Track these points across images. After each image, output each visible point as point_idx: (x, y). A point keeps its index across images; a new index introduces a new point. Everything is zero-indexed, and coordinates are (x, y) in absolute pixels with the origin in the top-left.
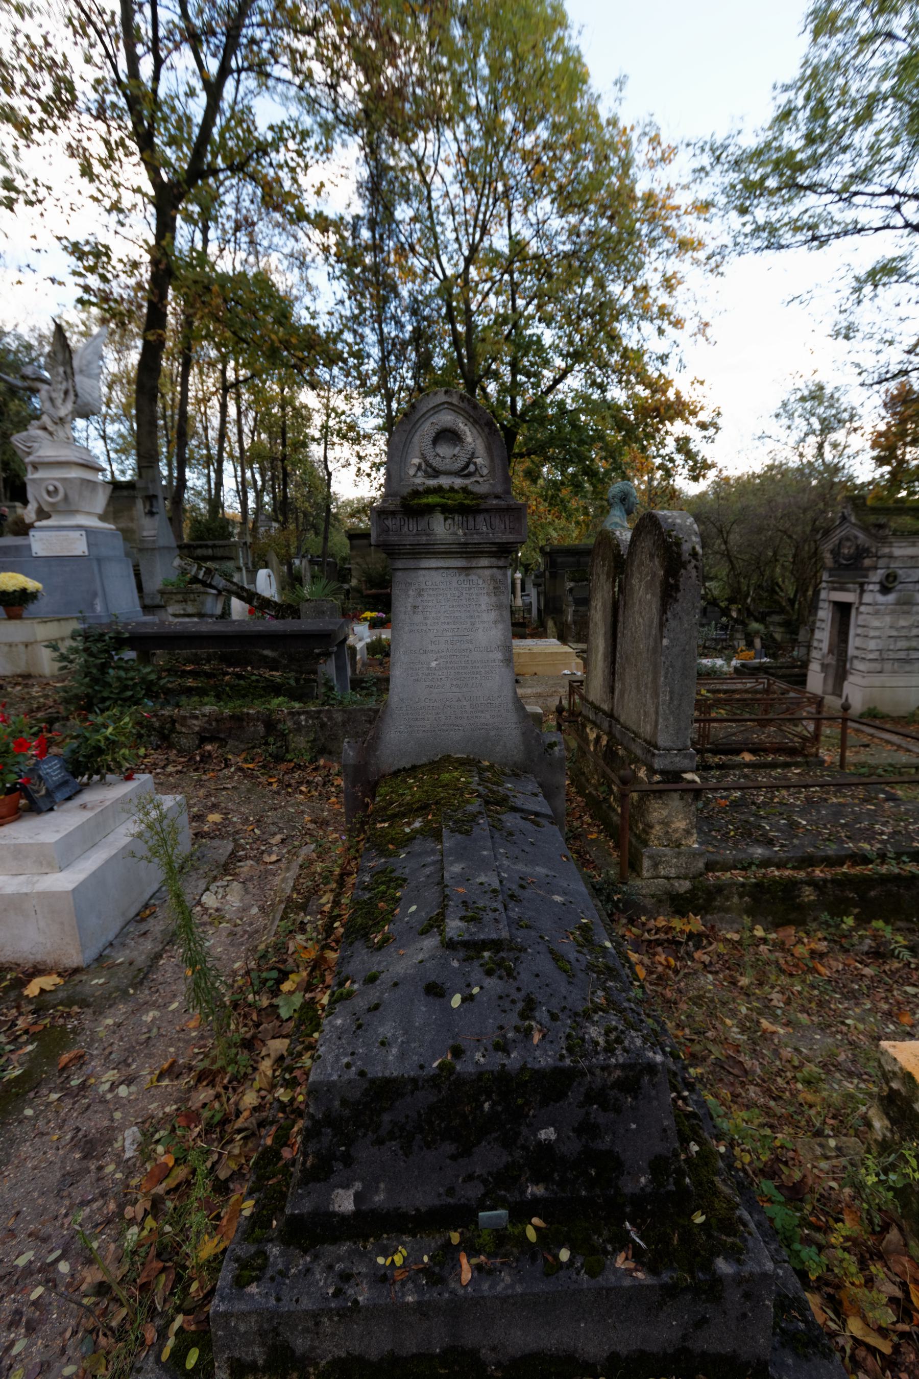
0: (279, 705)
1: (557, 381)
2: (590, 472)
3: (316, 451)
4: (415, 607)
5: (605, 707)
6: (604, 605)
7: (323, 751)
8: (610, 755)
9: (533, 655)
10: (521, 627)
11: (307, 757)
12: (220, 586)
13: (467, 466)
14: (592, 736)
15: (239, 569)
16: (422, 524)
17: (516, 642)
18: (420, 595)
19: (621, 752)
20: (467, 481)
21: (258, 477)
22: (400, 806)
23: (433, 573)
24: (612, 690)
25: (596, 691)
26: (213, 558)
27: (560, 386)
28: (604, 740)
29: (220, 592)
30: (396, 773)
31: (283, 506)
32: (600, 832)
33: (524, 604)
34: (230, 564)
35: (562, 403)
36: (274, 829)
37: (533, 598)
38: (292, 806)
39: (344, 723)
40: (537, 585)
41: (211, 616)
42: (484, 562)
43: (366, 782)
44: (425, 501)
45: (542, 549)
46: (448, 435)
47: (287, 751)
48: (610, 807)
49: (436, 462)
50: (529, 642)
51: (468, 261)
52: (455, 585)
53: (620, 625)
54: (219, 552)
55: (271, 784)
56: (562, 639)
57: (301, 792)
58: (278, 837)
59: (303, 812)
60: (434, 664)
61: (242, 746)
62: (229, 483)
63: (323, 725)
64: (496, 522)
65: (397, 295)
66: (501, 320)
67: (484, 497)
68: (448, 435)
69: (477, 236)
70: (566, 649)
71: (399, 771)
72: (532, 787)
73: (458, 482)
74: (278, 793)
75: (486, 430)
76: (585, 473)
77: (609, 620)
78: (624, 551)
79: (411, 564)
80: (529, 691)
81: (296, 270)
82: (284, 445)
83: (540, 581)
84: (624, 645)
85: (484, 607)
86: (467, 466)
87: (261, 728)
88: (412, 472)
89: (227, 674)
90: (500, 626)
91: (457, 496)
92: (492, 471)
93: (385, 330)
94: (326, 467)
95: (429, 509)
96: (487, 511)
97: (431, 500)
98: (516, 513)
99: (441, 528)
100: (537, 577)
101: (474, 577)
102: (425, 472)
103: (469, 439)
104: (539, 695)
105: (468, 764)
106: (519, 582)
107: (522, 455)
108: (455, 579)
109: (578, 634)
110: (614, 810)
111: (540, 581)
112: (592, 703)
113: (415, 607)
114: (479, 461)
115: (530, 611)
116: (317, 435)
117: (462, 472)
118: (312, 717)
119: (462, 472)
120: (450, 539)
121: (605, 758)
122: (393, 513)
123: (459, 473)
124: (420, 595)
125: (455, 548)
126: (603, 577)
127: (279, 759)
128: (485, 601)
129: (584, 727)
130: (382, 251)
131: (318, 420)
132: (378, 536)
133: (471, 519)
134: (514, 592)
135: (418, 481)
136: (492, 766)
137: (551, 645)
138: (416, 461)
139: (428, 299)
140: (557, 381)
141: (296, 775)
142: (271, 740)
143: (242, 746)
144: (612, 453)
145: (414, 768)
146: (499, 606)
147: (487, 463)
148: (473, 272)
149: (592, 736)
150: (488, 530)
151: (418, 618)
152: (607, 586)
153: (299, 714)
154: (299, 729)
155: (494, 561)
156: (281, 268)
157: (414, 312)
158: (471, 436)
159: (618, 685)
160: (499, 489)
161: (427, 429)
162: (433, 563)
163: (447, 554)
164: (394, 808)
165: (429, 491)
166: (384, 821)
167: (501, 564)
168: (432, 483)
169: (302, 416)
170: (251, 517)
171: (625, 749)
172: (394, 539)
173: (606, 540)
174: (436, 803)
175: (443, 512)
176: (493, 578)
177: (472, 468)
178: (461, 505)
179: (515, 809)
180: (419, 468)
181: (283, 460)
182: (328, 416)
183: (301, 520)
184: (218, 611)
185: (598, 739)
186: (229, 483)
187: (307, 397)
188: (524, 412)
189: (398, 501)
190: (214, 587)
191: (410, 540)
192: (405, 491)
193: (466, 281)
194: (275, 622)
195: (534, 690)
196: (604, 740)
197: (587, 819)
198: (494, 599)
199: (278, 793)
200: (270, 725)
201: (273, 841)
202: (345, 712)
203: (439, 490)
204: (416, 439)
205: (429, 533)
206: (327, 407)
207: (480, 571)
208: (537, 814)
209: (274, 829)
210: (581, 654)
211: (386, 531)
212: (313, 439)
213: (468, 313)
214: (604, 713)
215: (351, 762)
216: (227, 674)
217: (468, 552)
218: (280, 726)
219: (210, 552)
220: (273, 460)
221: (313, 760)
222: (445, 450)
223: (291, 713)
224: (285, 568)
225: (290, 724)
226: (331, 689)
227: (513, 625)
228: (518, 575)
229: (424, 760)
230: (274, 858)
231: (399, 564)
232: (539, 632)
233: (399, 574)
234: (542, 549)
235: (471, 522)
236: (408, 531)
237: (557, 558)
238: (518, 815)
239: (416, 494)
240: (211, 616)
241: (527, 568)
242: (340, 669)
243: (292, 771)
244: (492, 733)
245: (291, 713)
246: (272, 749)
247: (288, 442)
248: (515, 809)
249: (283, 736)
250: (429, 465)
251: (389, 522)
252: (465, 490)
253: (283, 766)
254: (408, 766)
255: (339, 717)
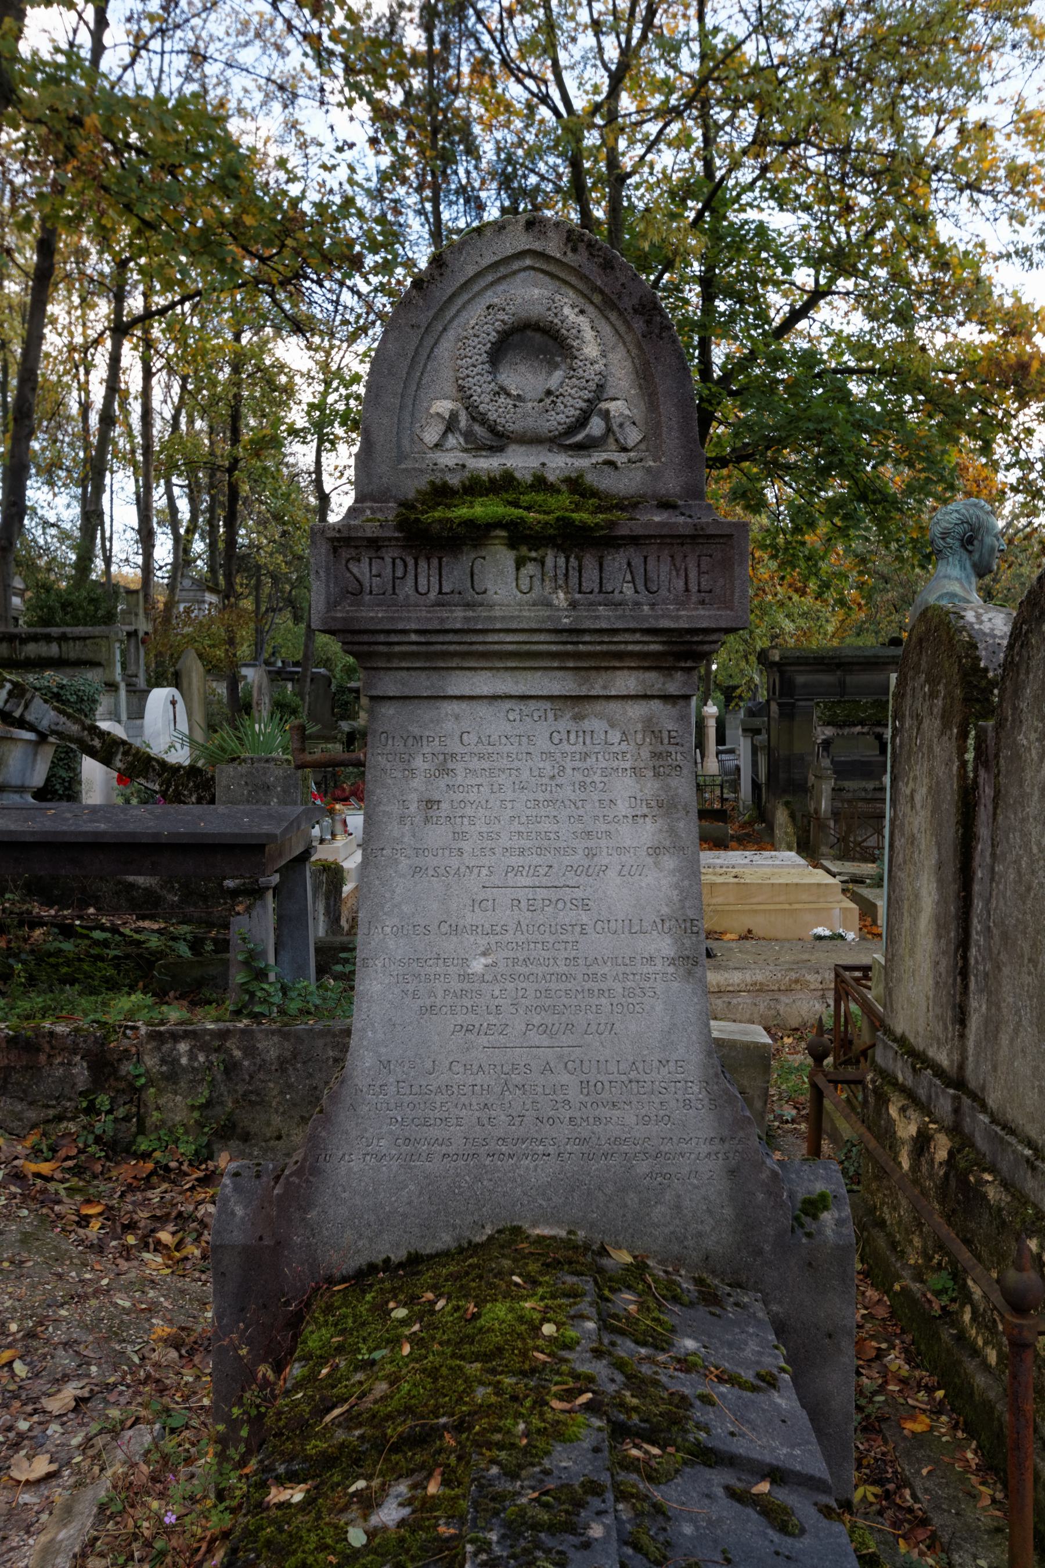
0: (131, 1015)
1: (796, 315)
2: (869, 493)
3: (301, 455)
4: (430, 803)
5: (943, 1058)
6: (935, 791)
7: (229, 1132)
8: (959, 1191)
9: (744, 888)
10: (722, 823)
11: (187, 1148)
12: (44, 725)
13: (583, 421)
14: (907, 1129)
15: (111, 686)
16: (455, 575)
17: (709, 857)
18: (444, 770)
19: (992, 1193)
20: (582, 462)
21: (183, 506)
22: (350, 1420)
23: (483, 710)
24: (961, 1018)
25: (915, 1005)
26: (58, 663)
27: (802, 325)
28: (941, 1149)
29: (43, 738)
30: (362, 1277)
31: (228, 559)
32: (937, 1410)
33: (724, 771)
34: (93, 676)
35: (809, 358)
36: (66, 1361)
37: (743, 759)
38: (128, 1288)
39: (283, 1065)
40: (751, 731)
41: (21, 789)
42: (627, 682)
43: (275, 1301)
44: (463, 512)
45: (762, 657)
46: (532, 339)
47: (141, 1130)
48: (961, 1337)
49: (497, 411)
50: (735, 858)
51: (617, 80)
52: (542, 743)
53: (982, 849)
54: (73, 651)
55: (84, 1221)
56: (807, 848)
57: (159, 1247)
58: (70, 1391)
59: (152, 1309)
60: (478, 965)
61: (32, 1115)
62: (121, 510)
63: (231, 1068)
64: (662, 571)
65: (473, 151)
66: (682, 193)
67: (630, 504)
68: (532, 339)
69: (637, 33)
70: (820, 876)
71: (372, 1268)
72: (758, 1350)
73: (558, 464)
74: (99, 1249)
75: (638, 324)
76: (863, 498)
77: (951, 833)
78: (991, 661)
79: (421, 683)
80: (736, 978)
81: (276, 106)
82: (235, 439)
83: (758, 722)
84: (997, 902)
85: (623, 808)
86: (583, 421)
87: (81, 1072)
88: (431, 436)
89: (36, 923)
90: (669, 862)
91: (552, 501)
92: (653, 433)
93: (445, 216)
94: (318, 483)
95: (475, 535)
96: (635, 540)
97: (481, 509)
98: (715, 547)
99: (507, 587)
100: (751, 713)
101: (596, 724)
102: (468, 435)
103: (591, 350)
104: (759, 989)
105: (571, 1261)
106: (712, 723)
107: (722, 462)
108: (542, 729)
109: (843, 839)
110: (976, 1352)
111: (758, 722)
112: (902, 1041)
113: (430, 803)
114: (615, 407)
115: (735, 786)
116: (301, 423)
117: (569, 438)
118: (204, 1048)
119: (569, 438)
120: (531, 617)
121: (943, 1195)
122: (375, 544)
123: (557, 441)
124: (444, 770)
125: (544, 643)
126: (932, 725)
127: (117, 1149)
128: (627, 790)
129: (883, 1100)
130: (447, 66)
131: (307, 393)
132: (332, 605)
133: (590, 562)
134: (700, 745)
135: (447, 460)
136: (640, 1267)
137: (783, 866)
138: (444, 406)
139: (535, 153)
140: (796, 315)
141: (154, 1196)
142: (103, 1100)
143: (32, 1115)
144: (918, 453)
145: (415, 1261)
146: (666, 806)
147: (638, 413)
148: (626, 103)
149: (907, 1129)
150: (636, 594)
151: (437, 835)
152: (943, 748)
153: (175, 1037)
154: (172, 1075)
155: (654, 681)
156: (247, 104)
157: (506, 181)
158: (592, 339)
159: (978, 1006)
160: (671, 484)
161: (477, 322)
162: (484, 683)
163: (524, 658)
164: (334, 1429)
165: (476, 487)
166: (292, 1478)
167: (673, 688)
168: (487, 464)
169: (276, 389)
170: (161, 577)
171: (1006, 1185)
172: (372, 614)
173: (940, 629)
174: (460, 1427)
175: (512, 544)
176: (651, 729)
177: (596, 426)
178: (564, 523)
179: (707, 1456)
180: (451, 425)
181: (231, 470)
182: (327, 383)
183: (266, 590)
184: (38, 778)
185: (922, 1143)
186: (121, 510)
187: (292, 353)
188: (728, 376)
189: (390, 512)
190: (31, 728)
191: (414, 619)
192: (412, 487)
193: (612, 116)
194: (141, 811)
195: (748, 977)
196: (941, 1149)
197: (895, 1361)
198: (651, 787)
199: (99, 1249)
200: (103, 1064)
201: (54, 1405)
202: (285, 1035)
203: (504, 484)
204: (446, 347)
205: (473, 598)
206: (325, 367)
207: (613, 706)
208: (777, 1475)
209: (66, 1361)
210: (852, 885)
211: (355, 592)
212: (293, 432)
213: (617, 179)
214: (939, 1072)
215: (237, 1237)
216: (36, 923)
217: (581, 653)
218: (127, 1068)
219: (54, 650)
220: (213, 470)
221: (204, 1155)
222: (522, 378)
223: (156, 1037)
224: (221, 689)
225: (150, 1061)
226: (261, 975)
227: (704, 814)
228: (711, 709)
229: (445, 1240)
230: (42, 1466)
231: (389, 685)
232: (757, 835)
233: (388, 710)
234: (762, 657)
235: (591, 574)
236: (417, 596)
237: (799, 681)
238: (719, 1478)
239: (441, 493)
240: (21, 789)
241: (729, 696)
242: (290, 923)
243: (148, 1182)
244: (643, 1167)
245: (156, 1037)
246: (104, 1124)
247: (246, 435)
248: (707, 1456)
249: (134, 1092)
250: (477, 417)
251: (362, 570)
252: (575, 484)
253: (127, 1170)
254: (398, 1255)
255: (271, 1049)
